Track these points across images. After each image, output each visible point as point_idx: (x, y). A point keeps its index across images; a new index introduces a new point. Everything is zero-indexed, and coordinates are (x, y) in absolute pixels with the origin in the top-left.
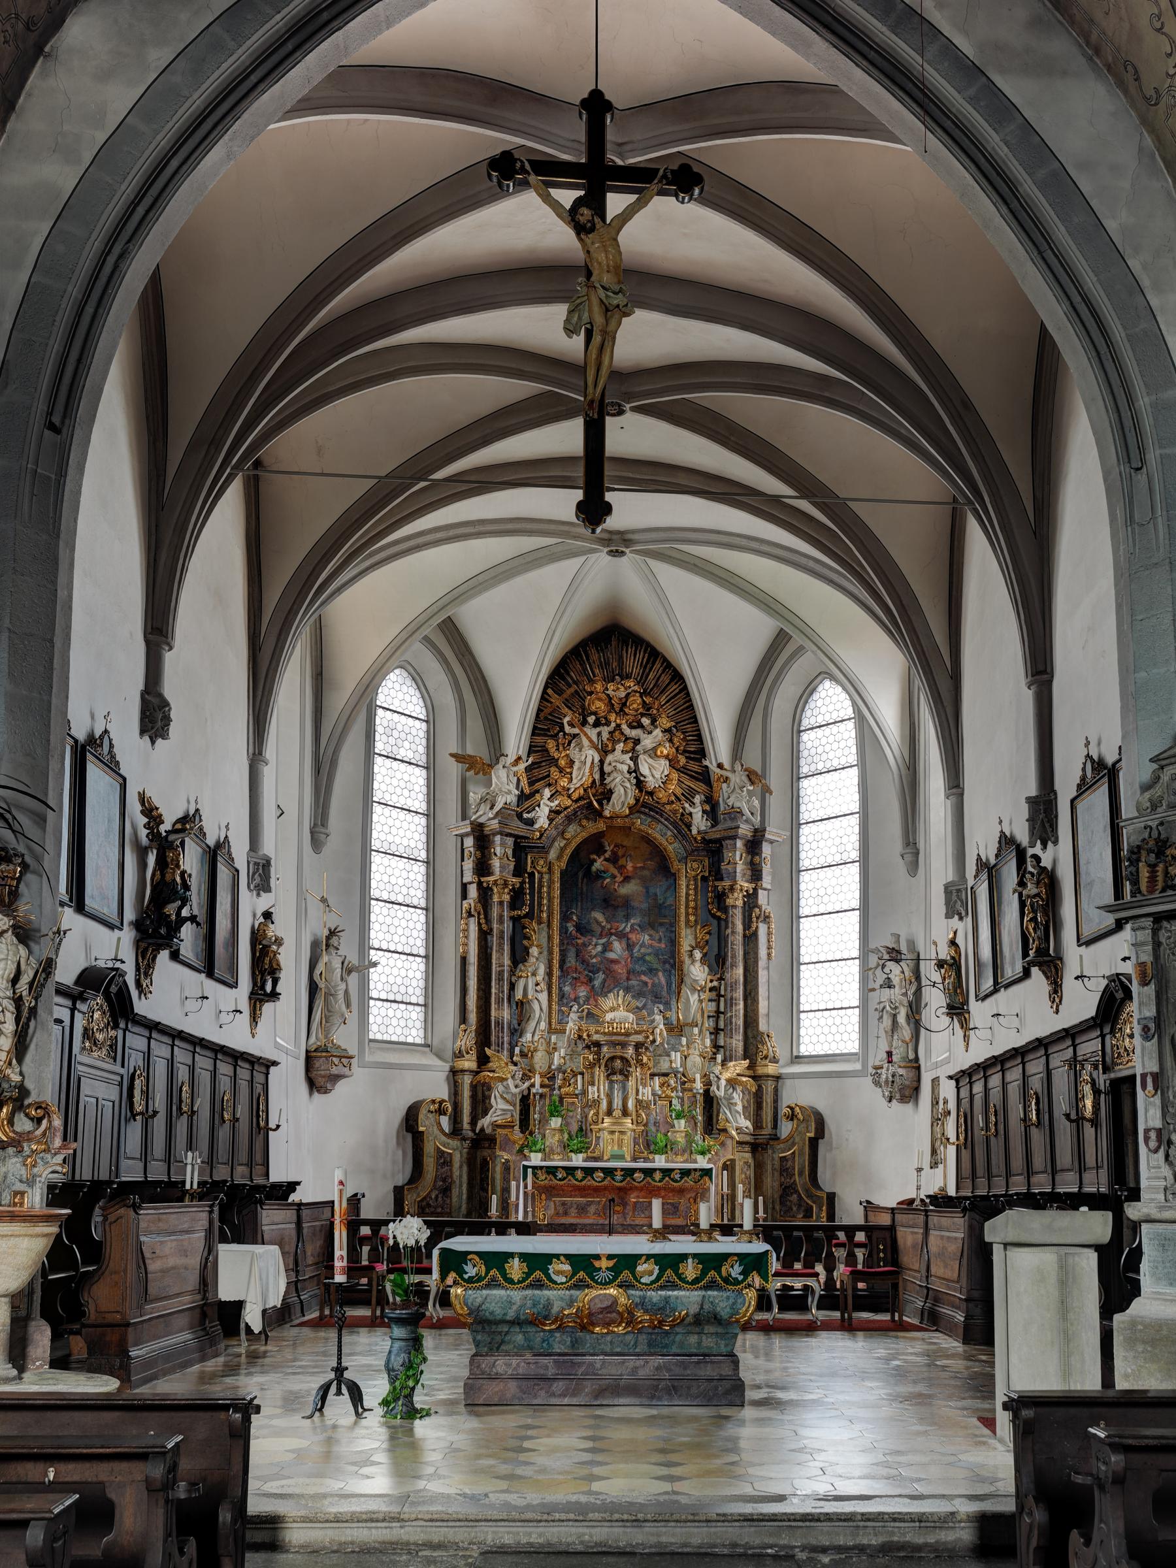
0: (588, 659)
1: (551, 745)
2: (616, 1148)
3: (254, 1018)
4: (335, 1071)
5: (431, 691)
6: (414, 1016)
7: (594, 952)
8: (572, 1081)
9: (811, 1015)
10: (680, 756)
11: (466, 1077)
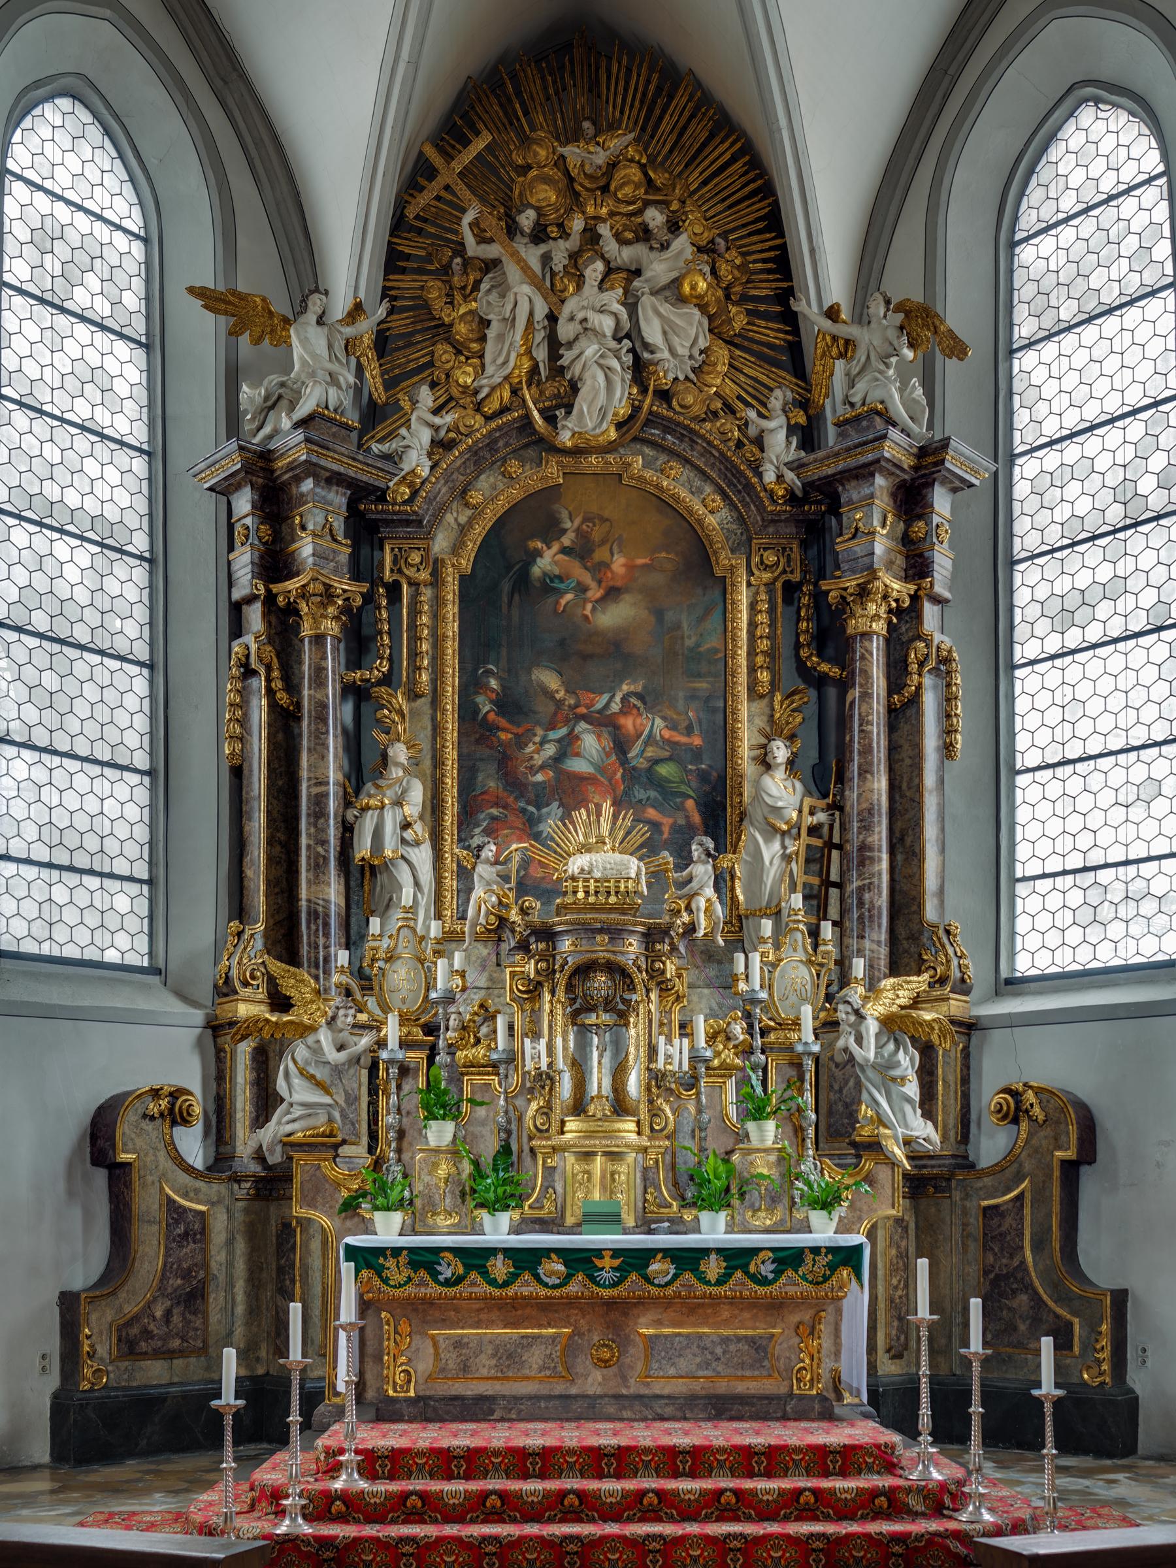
0: (518, 94)
1: (435, 292)
2: (597, 1195)
5: (152, 163)
6: (122, 903)
7: (538, 760)
8: (484, 1030)
9: (1044, 885)
10: (734, 310)
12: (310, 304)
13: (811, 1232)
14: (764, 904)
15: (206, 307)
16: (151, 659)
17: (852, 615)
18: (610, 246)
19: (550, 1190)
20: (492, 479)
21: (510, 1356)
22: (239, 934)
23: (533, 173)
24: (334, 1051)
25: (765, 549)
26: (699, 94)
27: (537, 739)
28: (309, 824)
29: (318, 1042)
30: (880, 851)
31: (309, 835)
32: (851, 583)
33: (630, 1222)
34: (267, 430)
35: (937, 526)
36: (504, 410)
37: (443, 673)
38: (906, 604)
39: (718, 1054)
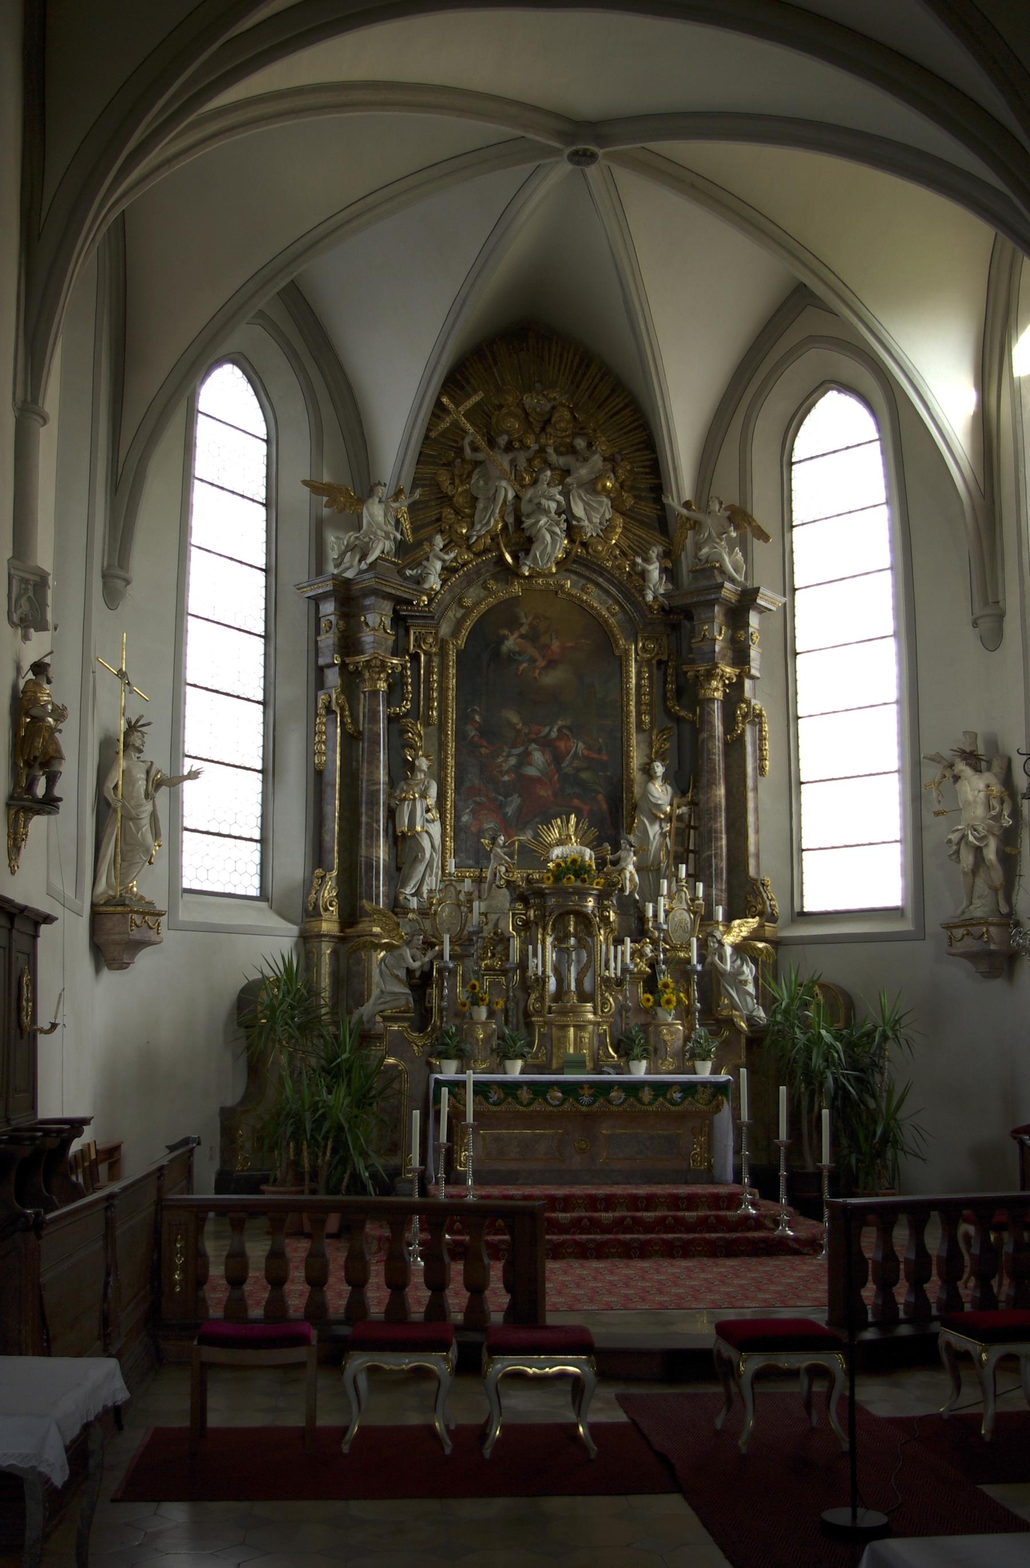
3: (15, 839)
4: (136, 934)
7: (505, 767)
11: (324, 945)
13: (696, 1074)
14: (650, 863)
16: (264, 699)
17: (702, 687)
18: (553, 457)
22: (323, 878)
23: (505, 410)
27: (505, 754)
30: (721, 833)
32: (702, 669)
33: (589, 1065)
37: (447, 711)
38: (734, 681)
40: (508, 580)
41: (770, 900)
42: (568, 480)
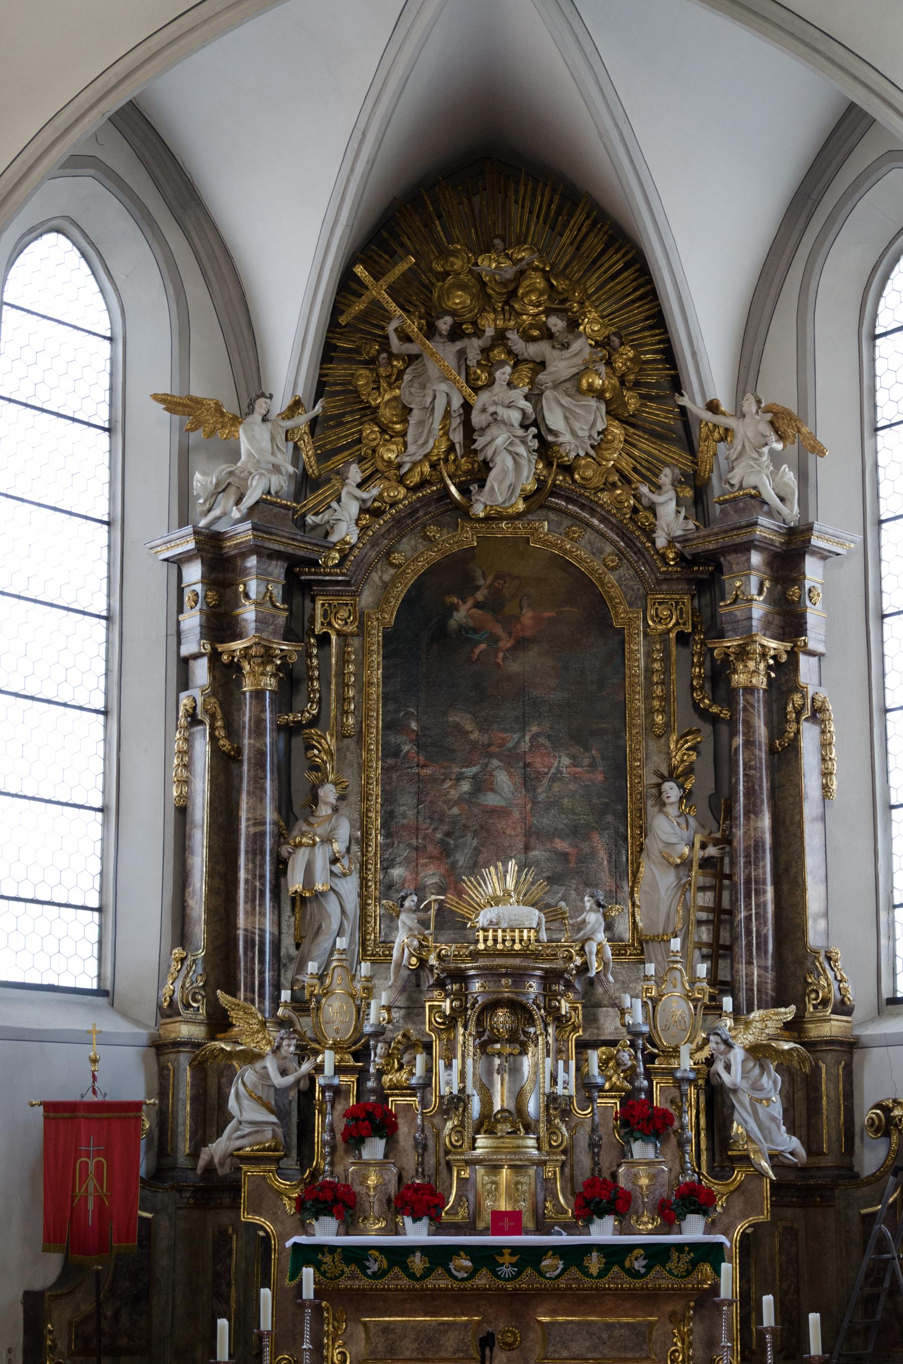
7: (454, 794)
12: (257, 406)
14: (661, 931)
15: (167, 409)
16: (106, 707)
17: (735, 671)
19: (464, 1199)
20: (413, 542)
21: (429, 1341)
22: (182, 960)
24: (279, 1076)
25: (660, 604)
26: (595, 213)
28: (247, 859)
29: (265, 1068)
30: (764, 883)
31: (247, 870)
33: (528, 1221)
34: (216, 512)
35: (810, 591)
36: (424, 483)
39: (609, 1078)
40: (457, 524)
41: (840, 981)
42: (541, 377)
